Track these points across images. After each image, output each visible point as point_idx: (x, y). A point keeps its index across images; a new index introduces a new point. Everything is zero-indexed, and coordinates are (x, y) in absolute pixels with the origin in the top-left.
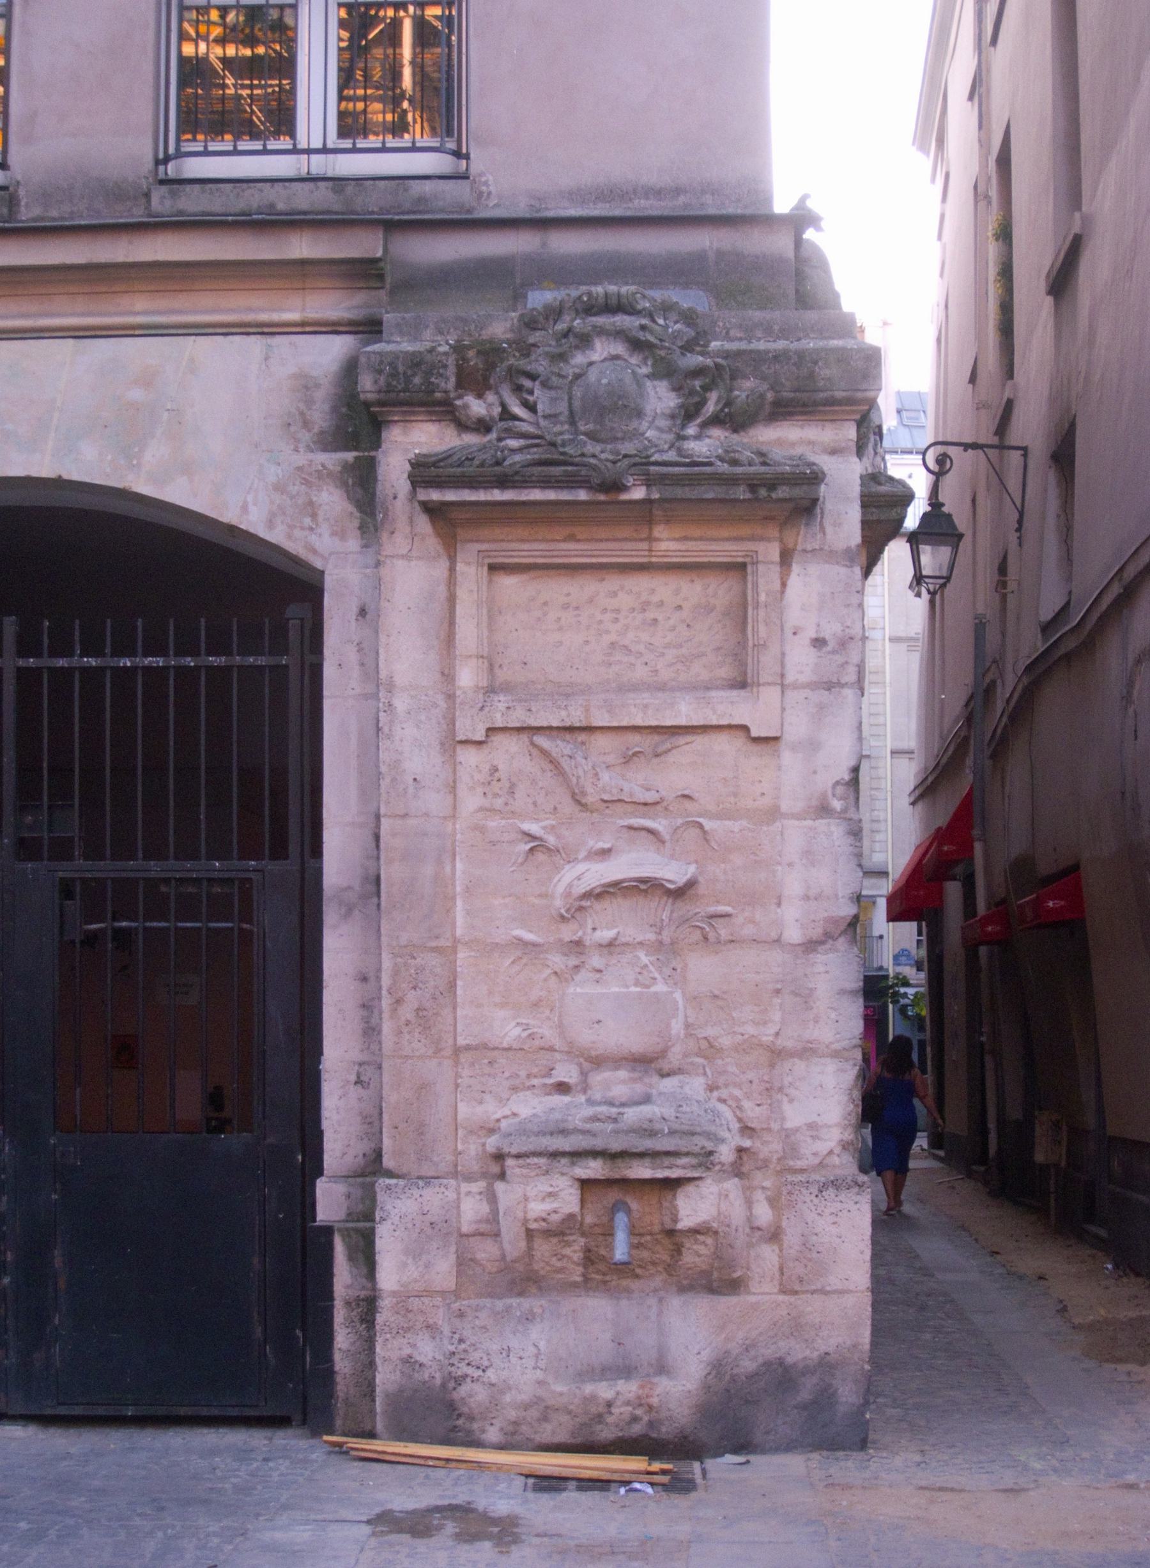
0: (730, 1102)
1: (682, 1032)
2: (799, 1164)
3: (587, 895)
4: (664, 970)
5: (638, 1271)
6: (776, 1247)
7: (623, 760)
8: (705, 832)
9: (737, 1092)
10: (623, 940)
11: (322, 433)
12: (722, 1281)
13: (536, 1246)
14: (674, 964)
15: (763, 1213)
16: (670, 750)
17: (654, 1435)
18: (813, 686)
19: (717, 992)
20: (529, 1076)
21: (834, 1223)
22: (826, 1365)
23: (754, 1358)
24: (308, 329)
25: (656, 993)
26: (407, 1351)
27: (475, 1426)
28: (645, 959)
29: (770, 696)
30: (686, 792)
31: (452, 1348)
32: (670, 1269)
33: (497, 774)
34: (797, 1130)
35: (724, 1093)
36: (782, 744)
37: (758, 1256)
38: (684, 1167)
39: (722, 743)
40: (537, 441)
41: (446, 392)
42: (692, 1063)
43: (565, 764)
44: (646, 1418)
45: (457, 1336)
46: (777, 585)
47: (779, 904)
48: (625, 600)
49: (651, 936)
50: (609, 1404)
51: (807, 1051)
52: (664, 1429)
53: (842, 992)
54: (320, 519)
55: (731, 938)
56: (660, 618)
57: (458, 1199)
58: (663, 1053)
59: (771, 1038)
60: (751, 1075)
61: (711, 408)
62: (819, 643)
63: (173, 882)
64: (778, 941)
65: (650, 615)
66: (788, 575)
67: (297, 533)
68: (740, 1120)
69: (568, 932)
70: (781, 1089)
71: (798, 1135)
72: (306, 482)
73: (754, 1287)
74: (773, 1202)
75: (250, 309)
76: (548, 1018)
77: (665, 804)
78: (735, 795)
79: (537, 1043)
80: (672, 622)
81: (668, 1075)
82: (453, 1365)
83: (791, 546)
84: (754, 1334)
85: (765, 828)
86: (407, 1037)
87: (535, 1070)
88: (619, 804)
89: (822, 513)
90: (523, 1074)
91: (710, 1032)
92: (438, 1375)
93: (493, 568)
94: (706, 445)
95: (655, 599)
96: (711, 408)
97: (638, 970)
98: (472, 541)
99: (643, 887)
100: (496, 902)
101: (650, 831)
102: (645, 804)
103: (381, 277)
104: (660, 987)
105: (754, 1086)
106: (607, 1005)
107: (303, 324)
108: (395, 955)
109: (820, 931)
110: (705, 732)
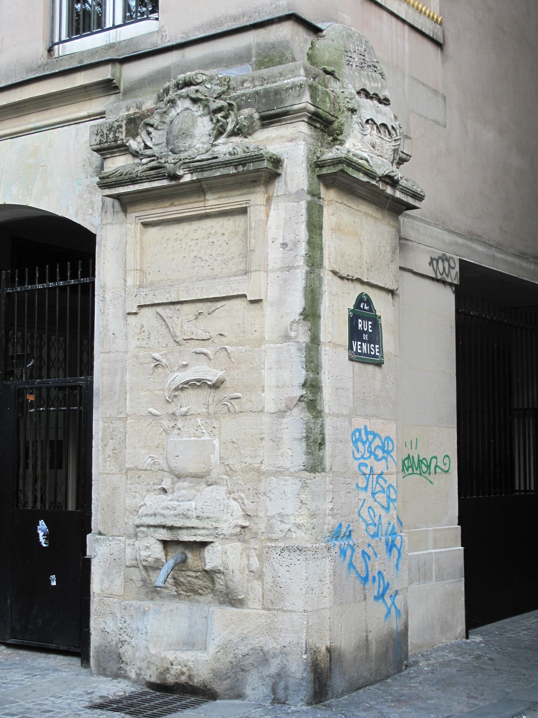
0: (239, 500)
1: (218, 461)
2: (275, 536)
3: (177, 389)
4: (209, 428)
5: (200, 591)
7: (195, 317)
8: (228, 353)
10: (190, 412)
11: (96, 167)
13: (151, 574)
14: (215, 425)
15: (255, 563)
16: (214, 311)
17: (191, 684)
19: (234, 440)
21: (288, 571)
22: (284, 652)
24: (92, 118)
30: (221, 333)
31: (121, 625)
32: (213, 590)
33: (143, 329)
35: (236, 495)
36: (264, 303)
37: (252, 587)
40: (152, 158)
41: (122, 140)
42: (221, 479)
44: (187, 674)
46: (263, 216)
54: (95, 209)
56: (215, 241)
57: (125, 547)
58: (209, 473)
59: (258, 465)
60: (249, 486)
61: (230, 128)
63: (68, 389)
66: (270, 211)
67: (87, 217)
69: (171, 408)
71: (274, 520)
72: (90, 192)
75: (71, 113)
78: (244, 332)
80: (220, 243)
81: (211, 485)
82: (120, 634)
83: (271, 195)
86: (109, 463)
87: (156, 481)
89: (286, 174)
90: (151, 483)
94: (225, 147)
96: (230, 128)
98: (133, 212)
99: (198, 384)
100: (142, 394)
101: (205, 354)
103: (117, 88)
104: (206, 438)
105: (250, 491)
107: (89, 116)
108: (104, 422)
109: (284, 405)
110: (230, 299)
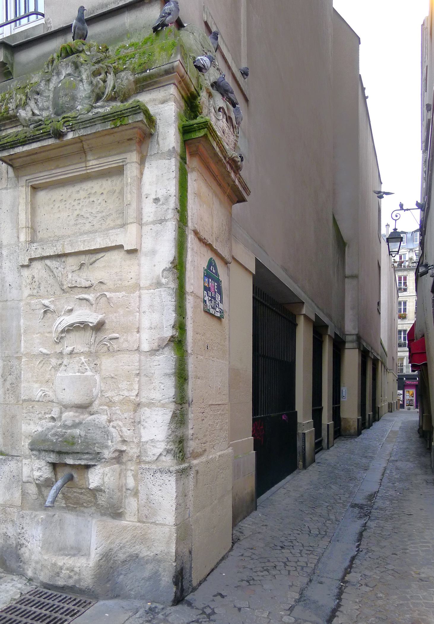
3: (63, 331)
4: (91, 364)
6: (136, 499)
9: (120, 423)
12: (116, 513)
18: (154, 223)
19: (113, 375)
20: (45, 413)
22: (156, 560)
23: (124, 553)
25: (87, 375)
26: (5, 530)
27: (26, 567)
28: (83, 359)
29: (133, 229)
34: (147, 442)
38: (86, 459)
39: (115, 256)
43: (55, 271)
45: (21, 526)
47: (138, 332)
48: (82, 194)
49: (87, 349)
50: (61, 568)
51: (151, 404)
52: (82, 584)
53: (166, 375)
55: (118, 349)
56: (95, 200)
58: (90, 404)
60: (126, 415)
62: (156, 200)
64: (138, 349)
65: (91, 199)
66: (144, 169)
68: (121, 437)
70: (139, 422)
73: (127, 516)
74: (135, 476)
76: (52, 388)
77: (93, 287)
78: (121, 280)
79: (48, 398)
80: (99, 201)
84: (124, 541)
85: (132, 295)
87: (47, 411)
88: (76, 289)
89: (158, 135)
90: (43, 412)
91: (109, 394)
92: (14, 542)
93: (35, 189)
95: (93, 191)
97: (80, 365)
101: (87, 300)
102: (86, 288)
106: (67, 383)
109: (156, 344)
110: (109, 251)
